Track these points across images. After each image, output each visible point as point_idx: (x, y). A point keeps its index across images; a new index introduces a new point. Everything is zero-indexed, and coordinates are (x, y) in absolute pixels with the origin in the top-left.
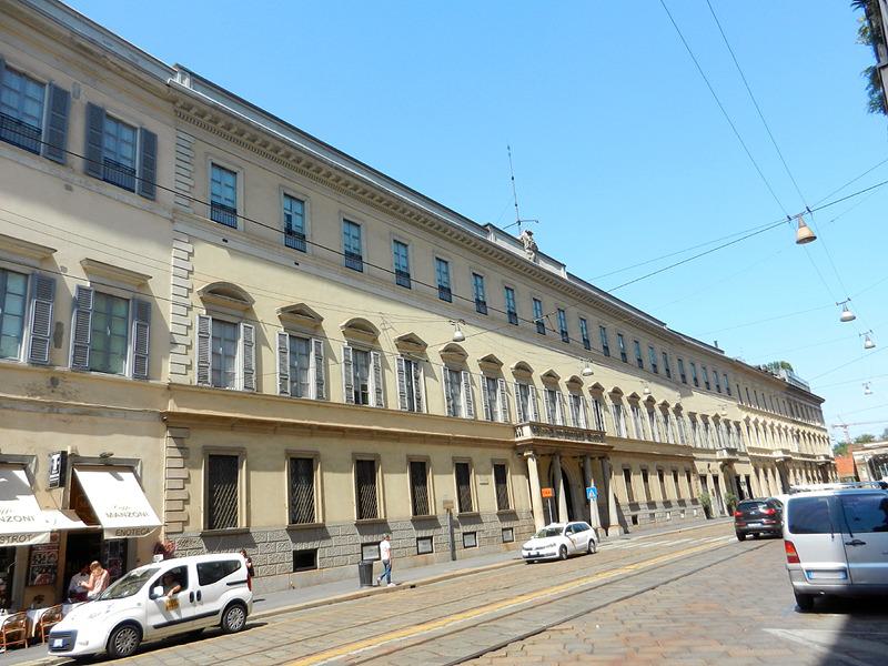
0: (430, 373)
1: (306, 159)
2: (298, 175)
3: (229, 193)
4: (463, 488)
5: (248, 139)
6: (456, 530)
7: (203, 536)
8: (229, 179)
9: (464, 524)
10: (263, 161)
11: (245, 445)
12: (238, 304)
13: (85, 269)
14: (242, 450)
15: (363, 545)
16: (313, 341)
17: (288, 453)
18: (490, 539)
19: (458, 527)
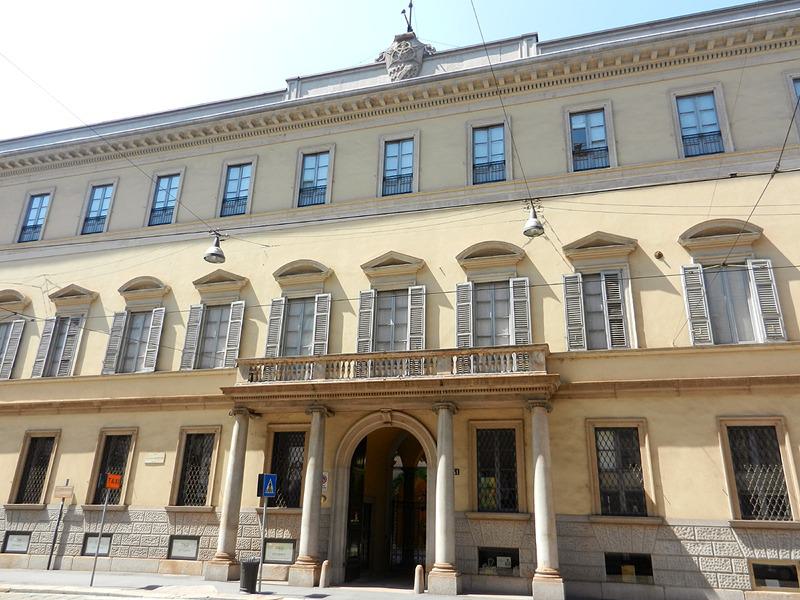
0: (448, 305)
1: (248, 119)
2: (282, 133)
3: (709, 118)
4: (756, 478)
5: (754, 40)
6: (73, 528)
7: (734, 526)
8: (705, 103)
9: (90, 522)
10: (432, 111)
11: (646, 415)
12: (156, 292)
13: (685, 247)
14: (644, 420)
15: (267, 541)
16: (750, 265)
17: (720, 419)
18: (143, 550)
19: (79, 523)
